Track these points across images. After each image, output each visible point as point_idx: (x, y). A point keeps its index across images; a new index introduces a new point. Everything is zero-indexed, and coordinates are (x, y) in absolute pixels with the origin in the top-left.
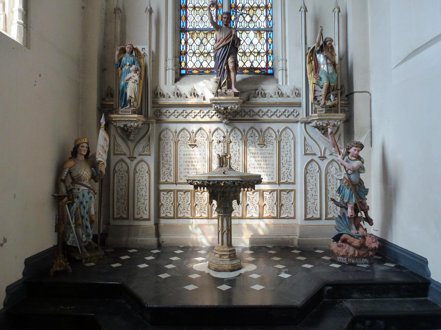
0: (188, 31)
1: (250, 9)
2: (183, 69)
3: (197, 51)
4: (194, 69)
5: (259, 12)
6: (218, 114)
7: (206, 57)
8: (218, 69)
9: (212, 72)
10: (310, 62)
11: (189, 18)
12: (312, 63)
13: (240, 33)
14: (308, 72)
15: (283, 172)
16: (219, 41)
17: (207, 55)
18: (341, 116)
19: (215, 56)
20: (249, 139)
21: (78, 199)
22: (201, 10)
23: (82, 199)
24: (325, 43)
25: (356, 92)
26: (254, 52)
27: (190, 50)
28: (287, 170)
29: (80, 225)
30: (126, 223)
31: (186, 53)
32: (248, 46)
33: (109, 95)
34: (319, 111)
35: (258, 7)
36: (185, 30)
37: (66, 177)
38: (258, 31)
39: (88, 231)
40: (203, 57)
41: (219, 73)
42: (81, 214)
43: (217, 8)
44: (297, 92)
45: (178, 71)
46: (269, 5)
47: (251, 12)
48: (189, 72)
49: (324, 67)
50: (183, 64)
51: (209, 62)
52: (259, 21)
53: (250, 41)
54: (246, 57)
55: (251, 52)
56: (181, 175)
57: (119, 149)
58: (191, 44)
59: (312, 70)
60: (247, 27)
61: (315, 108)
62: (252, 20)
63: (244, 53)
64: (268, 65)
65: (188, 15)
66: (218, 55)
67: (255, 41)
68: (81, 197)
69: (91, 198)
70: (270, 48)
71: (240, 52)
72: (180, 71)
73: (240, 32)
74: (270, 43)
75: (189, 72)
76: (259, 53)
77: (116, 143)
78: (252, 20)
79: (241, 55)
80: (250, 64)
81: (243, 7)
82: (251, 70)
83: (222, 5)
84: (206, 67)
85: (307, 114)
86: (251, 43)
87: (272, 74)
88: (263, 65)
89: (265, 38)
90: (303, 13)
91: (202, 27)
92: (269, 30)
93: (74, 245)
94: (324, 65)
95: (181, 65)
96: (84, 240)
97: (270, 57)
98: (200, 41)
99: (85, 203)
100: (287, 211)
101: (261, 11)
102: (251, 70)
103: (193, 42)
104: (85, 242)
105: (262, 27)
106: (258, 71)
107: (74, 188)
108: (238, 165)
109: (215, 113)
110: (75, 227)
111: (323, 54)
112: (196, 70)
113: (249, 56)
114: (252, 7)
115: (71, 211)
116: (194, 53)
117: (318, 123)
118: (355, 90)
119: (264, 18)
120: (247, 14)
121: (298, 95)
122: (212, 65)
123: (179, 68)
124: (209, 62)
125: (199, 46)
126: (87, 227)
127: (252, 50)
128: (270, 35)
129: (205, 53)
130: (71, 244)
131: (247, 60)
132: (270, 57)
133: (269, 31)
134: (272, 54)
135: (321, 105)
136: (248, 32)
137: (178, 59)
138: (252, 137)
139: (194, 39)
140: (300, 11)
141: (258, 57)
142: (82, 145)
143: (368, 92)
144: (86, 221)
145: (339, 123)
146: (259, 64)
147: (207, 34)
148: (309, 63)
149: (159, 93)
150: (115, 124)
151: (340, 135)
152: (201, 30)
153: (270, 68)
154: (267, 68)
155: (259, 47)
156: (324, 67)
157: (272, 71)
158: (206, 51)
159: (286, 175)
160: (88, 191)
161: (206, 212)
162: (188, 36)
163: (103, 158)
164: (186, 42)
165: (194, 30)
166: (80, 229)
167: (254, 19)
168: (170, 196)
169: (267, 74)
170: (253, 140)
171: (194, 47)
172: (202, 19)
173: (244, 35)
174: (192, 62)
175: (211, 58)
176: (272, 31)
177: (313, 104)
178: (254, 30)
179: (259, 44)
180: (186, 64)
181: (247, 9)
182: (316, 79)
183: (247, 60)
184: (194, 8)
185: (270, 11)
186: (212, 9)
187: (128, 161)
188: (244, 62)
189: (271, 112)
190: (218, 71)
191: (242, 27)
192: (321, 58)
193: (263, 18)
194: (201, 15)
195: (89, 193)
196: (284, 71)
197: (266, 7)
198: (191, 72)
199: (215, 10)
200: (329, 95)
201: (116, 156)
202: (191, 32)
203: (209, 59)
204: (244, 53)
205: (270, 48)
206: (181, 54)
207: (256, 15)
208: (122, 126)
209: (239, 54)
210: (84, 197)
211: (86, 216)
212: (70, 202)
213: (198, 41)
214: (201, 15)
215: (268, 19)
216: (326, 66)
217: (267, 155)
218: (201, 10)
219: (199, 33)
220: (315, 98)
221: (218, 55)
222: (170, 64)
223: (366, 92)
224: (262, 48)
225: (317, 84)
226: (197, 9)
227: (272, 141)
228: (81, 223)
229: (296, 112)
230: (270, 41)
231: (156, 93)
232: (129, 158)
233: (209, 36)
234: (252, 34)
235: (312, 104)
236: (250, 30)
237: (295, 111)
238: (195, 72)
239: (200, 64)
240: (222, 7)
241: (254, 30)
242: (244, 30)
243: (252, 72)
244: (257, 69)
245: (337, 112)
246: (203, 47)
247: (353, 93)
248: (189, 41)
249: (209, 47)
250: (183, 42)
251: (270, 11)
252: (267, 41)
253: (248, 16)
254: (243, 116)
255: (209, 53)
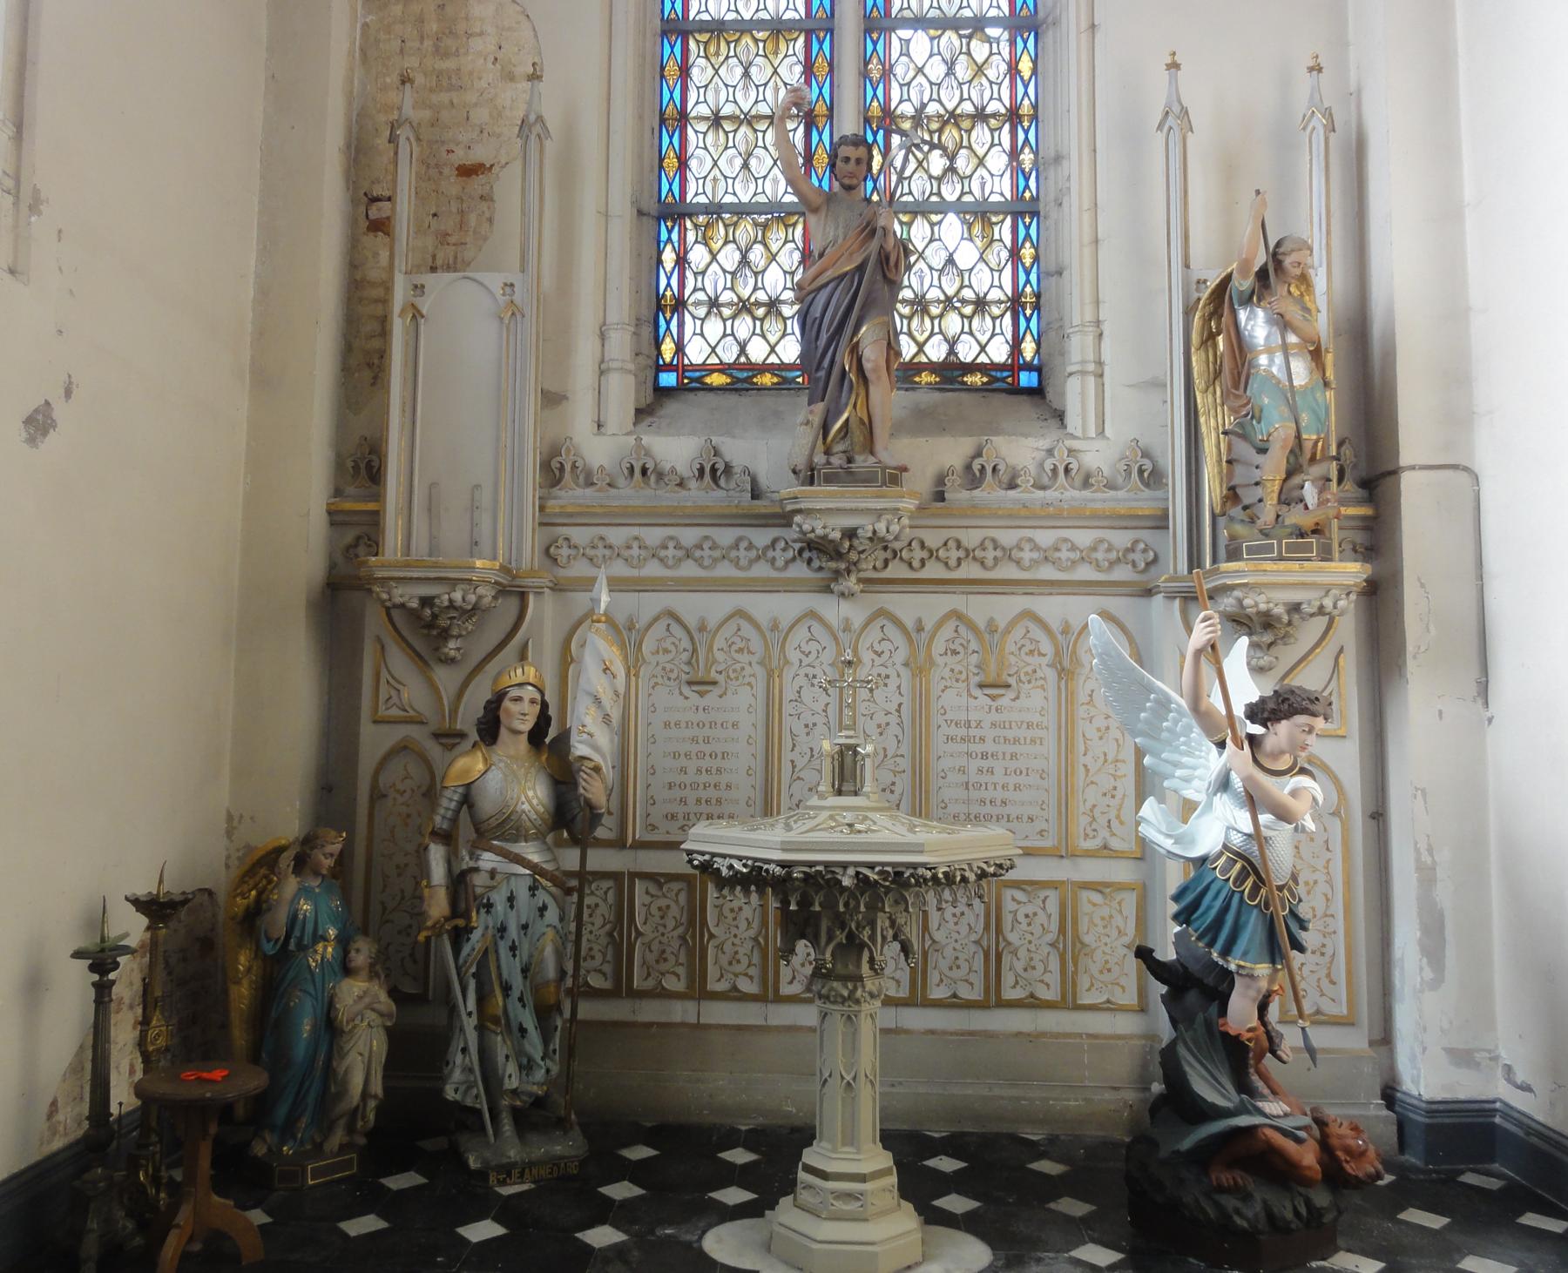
0: (690, 216)
1: (945, 123)
2: (669, 367)
3: (727, 296)
4: (711, 370)
5: (981, 135)
6: (814, 554)
7: (762, 320)
8: (818, 369)
9: (785, 380)
10: (1209, 338)
11: (693, 163)
12: (1215, 346)
13: (901, 223)
14: (1199, 382)
15: (1089, 805)
16: (821, 255)
17: (768, 313)
18: (1353, 572)
19: (804, 317)
20: (940, 660)
21: (488, 912)
22: (744, 129)
23: (505, 914)
24: (1276, 257)
25: (1413, 468)
26: (964, 302)
27: (695, 290)
28: (1107, 800)
29: (496, 1021)
30: (682, 1012)
31: (680, 304)
32: (936, 274)
33: (363, 471)
34: (1250, 550)
35: (980, 116)
36: (677, 212)
37: (454, 821)
38: (979, 214)
39: (528, 1048)
40: (749, 319)
41: (821, 384)
42: (500, 976)
43: (810, 121)
44: (1148, 466)
45: (650, 373)
46: (1026, 108)
47: (950, 136)
48: (693, 382)
49: (1271, 361)
50: (668, 349)
51: (773, 340)
52: (981, 171)
53: (944, 255)
54: (927, 321)
55: (948, 299)
56: (651, 810)
57: (395, 699)
58: (702, 267)
59: (1218, 374)
60: (934, 199)
61: (1232, 538)
62: (951, 169)
63: (920, 303)
64: (1020, 352)
65: (690, 150)
66: (816, 311)
67: (967, 255)
68: (500, 906)
69: (543, 909)
70: (1028, 281)
71: (904, 301)
72: (656, 378)
73: (905, 218)
74: (1028, 261)
75: (692, 380)
76: (981, 304)
77: (384, 675)
78: (951, 169)
79: (906, 311)
80: (945, 348)
81: (918, 118)
82: (949, 374)
83: (831, 109)
84: (760, 361)
85: (1194, 560)
86: (951, 261)
87: (1037, 392)
88: (999, 352)
89: (1008, 243)
90: (1175, 137)
91: (745, 199)
92: (1023, 209)
93: (469, 1102)
94: (1270, 351)
95: (659, 354)
96: (512, 1083)
97: (1028, 320)
98: (737, 256)
99: (513, 932)
100: (1106, 977)
101: (992, 131)
102: (949, 374)
103: (708, 258)
104: (514, 1092)
105: (995, 198)
106: (976, 379)
107: (477, 870)
108: (895, 773)
109: (801, 551)
110: (480, 1028)
111: (1264, 309)
112: (722, 371)
113: (941, 316)
114: (953, 118)
115: (461, 961)
116: (714, 304)
117: (1247, 602)
118: (1405, 459)
119: (1005, 159)
120: (933, 147)
121: (1153, 477)
122: (790, 351)
123: (651, 362)
124: (773, 340)
125: (733, 274)
126: (523, 1031)
127: (950, 292)
128: (1027, 228)
129: (758, 304)
130: (458, 1097)
131: (932, 334)
132: (1028, 320)
133: (1022, 214)
134: (1037, 307)
135: (1259, 523)
136: (935, 218)
137: (647, 331)
138: (955, 652)
139: (715, 246)
140: (1160, 127)
141: (976, 322)
142: (514, 693)
143: (1466, 469)
144: (519, 1005)
145: (1341, 603)
146: (983, 349)
147: (765, 227)
148: (1204, 343)
149: (568, 468)
150: (385, 596)
151: (1341, 650)
152: (741, 211)
153: (1028, 367)
154: (1016, 364)
155: (982, 281)
156: (1271, 361)
157: (1035, 375)
158: (761, 296)
159: (1102, 821)
160: (529, 882)
161: (681, 971)
162: (691, 236)
163: (596, 748)
164: (682, 261)
165: (715, 210)
166: (499, 1038)
167: (961, 163)
168: (1044, 909)
169: (1016, 390)
170: (958, 668)
171: (715, 281)
172: (746, 166)
173: (919, 232)
174: (703, 342)
175: (781, 326)
176: (1035, 214)
177: (1222, 521)
178: (959, 208)
179: (981, 265)
180: (680, 348)
181: (935, 126)
182: (1234, 411)
183: (932, 334)
184: (716, 120)
185: (1026, 132)
186: (790, 125)
187: (434, 750)
188: (921, 339)
189: (1109, 550)
190: (818, 380)
191: (910, 199)
192: (1256, 325)
193: (998, 161)
194: (742, 150)
195: (533, 889)
196: (1091, 380)
197: (1013, 116)
198: (699, 380)
199: (801, 129)
200: (1296, 480)
201: (385, 728)
202: (702, 219)
203: (773, 328)
204: (921, 305)
205: (1028, 281)
206: (660, 308)
207: (970, 147)
208: (414, 604)
209: (899, 306)
210: (512, 907)
211: (518, 983)
212: (461, 922)
213: (729, 258)
214: (742, 150)
215: (1020, 164)
216: (1279, 358)
217: (1021, 733)
218: (744, 129)
219: (735, 224)
220: (1232, 495)
221: (816, 311)
222: (621, 345)
223: (1455, 467)
224: (993, 282)
225: (1240, 432)
226: (728, 126)
227: (1040, 674)
228: (500, 1012)
229: (1145, 551)
230: (1027, 253)
231: (555, 464)
232: (437, 736)
233: (776, 236)
234: (952, 226)
235: (1214, 517)
236: (943, 208)
237: (1142, 546)
238: (717, 379)
239: (736, 350)
240: (830, 117)
241: (959, 208)
242: (920, 210)
243: (952, 381)
244: (972, 368)
245: (1326, 555)
246: (751, 281)
247: (1395, 472)
248: (692, 256)
249: (775, 282)
250: (669, 257)
251: (1026, 132)
252: (1015, 254)
253: (937, 153)
254: (953, 563)
255: (773, 305)
